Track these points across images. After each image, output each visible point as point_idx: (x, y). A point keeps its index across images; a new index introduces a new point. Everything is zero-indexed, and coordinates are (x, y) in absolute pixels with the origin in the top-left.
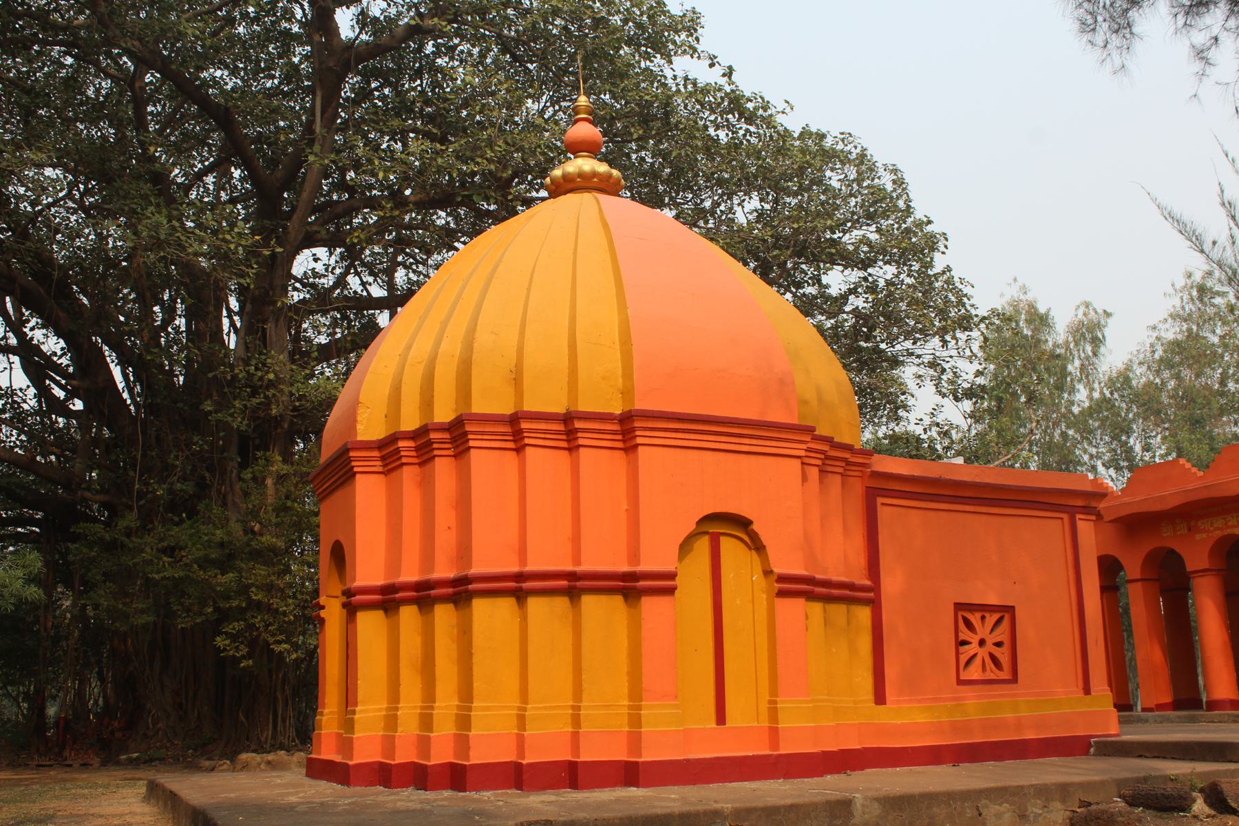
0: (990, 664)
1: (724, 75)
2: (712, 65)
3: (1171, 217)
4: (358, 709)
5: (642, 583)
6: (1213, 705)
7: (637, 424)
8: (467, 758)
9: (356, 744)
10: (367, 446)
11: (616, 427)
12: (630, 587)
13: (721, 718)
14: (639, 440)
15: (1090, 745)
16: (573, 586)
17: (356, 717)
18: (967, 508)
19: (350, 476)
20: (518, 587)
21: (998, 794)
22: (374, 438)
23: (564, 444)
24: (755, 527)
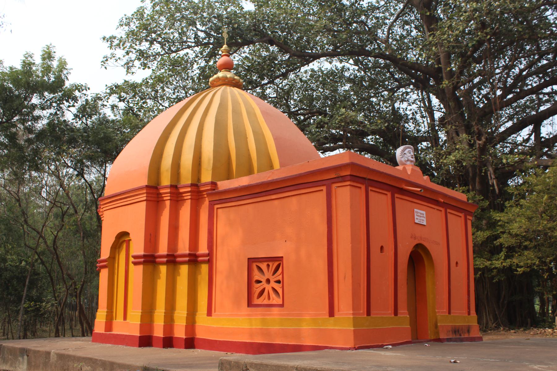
13: (125, 318)
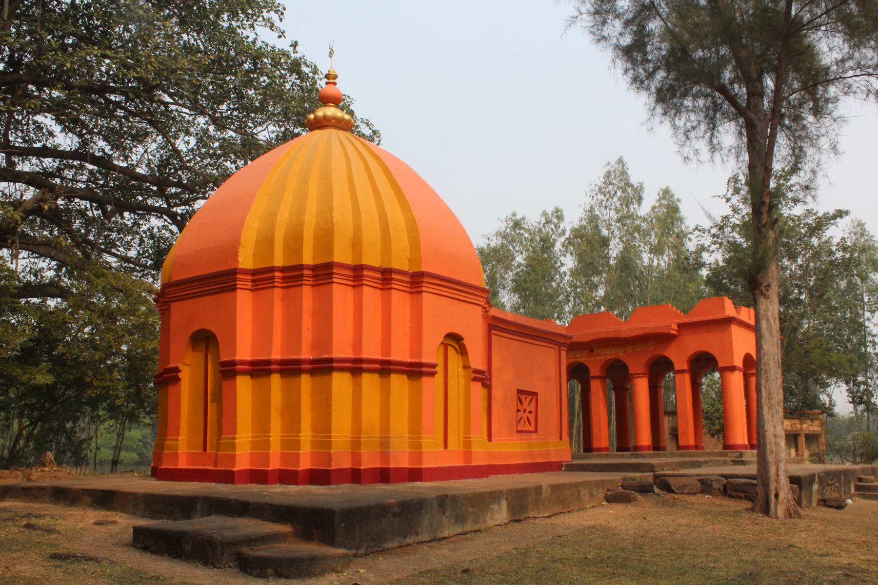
0: (527, 423)
1: (291, 46)
2: (280, 37)
3: (706, 212)
4: (237, 436)
5: (424, 369)
6: (600, 450)
7: (425, 280)
8: (330, 465)
9: (238, 459)
10: (245, 272)
11: (408, 279)
12: (416, 371)
13: (446, 446)
14: (424, 289)
15: (562, 466)
16: (385, 368)
17: (237, 441)
18: (533, 341)
19: (234, 289)
20: (356, 367)
21: (586, 484)
22: (248, 267)
23: (380, 286)
24: (465, 342)
